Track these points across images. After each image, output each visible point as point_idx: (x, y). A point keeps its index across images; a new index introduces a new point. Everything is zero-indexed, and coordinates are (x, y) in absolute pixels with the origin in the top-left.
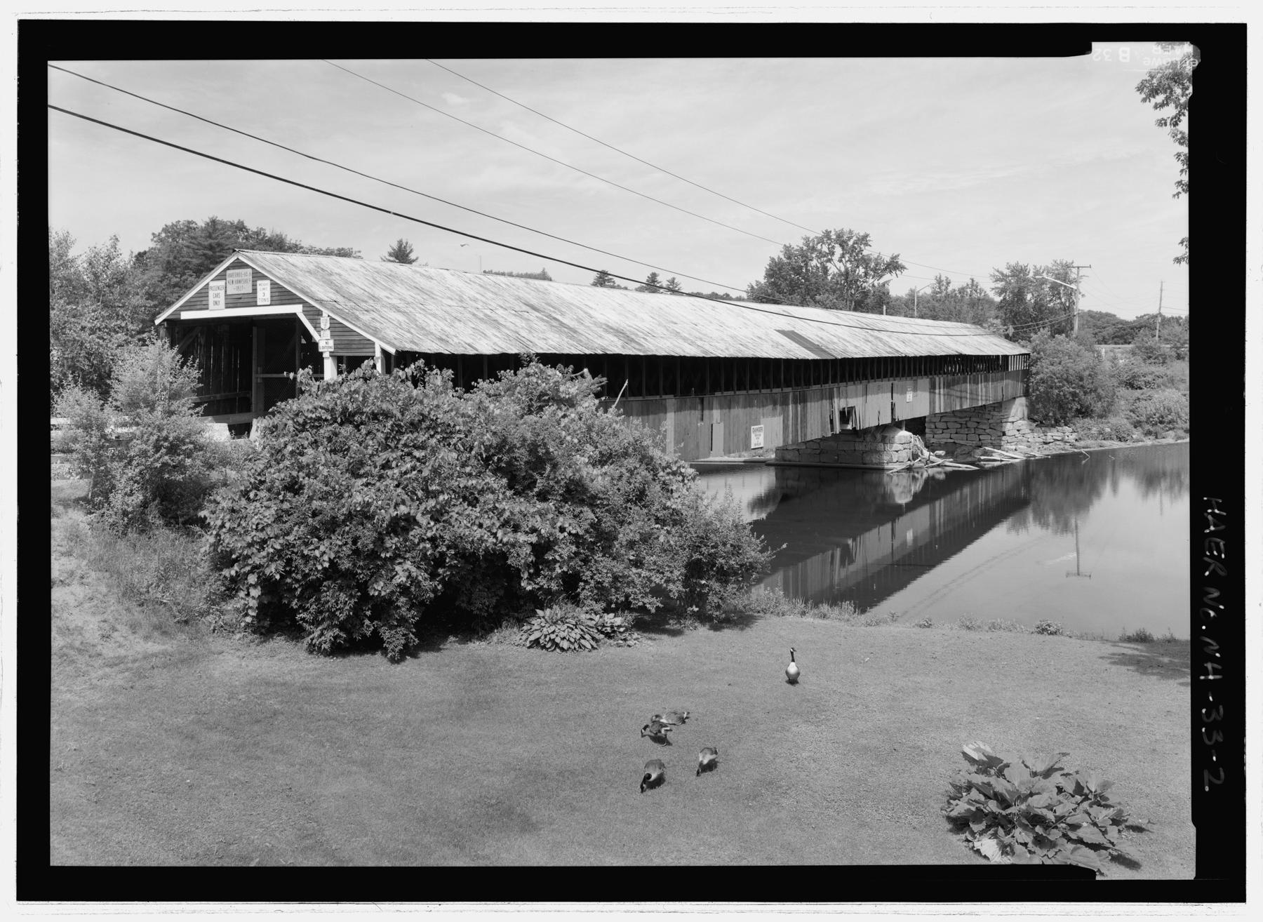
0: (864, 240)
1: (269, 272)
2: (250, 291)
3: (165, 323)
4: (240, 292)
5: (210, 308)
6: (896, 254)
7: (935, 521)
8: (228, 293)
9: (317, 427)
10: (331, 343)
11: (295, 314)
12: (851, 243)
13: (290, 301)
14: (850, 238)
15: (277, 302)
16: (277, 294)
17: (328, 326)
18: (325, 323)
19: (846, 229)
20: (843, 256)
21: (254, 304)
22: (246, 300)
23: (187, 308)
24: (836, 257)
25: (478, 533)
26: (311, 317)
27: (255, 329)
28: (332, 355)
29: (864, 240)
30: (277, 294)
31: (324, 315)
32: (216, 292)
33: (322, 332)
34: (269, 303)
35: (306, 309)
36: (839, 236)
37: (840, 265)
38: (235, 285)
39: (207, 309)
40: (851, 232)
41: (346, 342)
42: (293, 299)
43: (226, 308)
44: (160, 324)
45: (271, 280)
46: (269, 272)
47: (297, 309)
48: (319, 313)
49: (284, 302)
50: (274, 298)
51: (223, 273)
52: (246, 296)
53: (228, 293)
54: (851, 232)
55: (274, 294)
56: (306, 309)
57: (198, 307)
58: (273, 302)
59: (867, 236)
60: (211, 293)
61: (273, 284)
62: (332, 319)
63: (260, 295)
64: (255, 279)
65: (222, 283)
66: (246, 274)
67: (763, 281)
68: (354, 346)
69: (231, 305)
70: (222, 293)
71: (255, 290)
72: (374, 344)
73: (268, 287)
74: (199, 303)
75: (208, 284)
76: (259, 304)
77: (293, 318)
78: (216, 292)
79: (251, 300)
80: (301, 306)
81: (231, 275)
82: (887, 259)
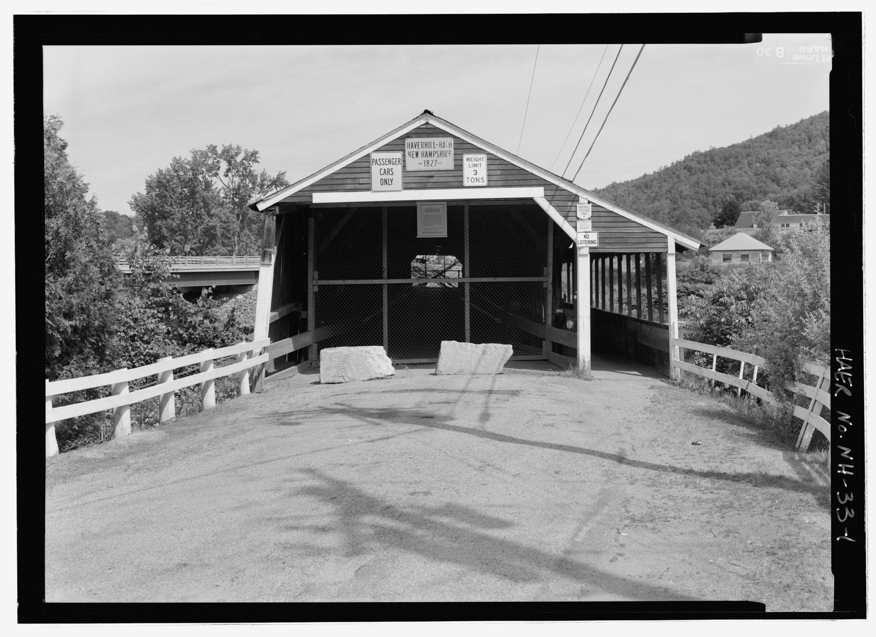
0: (253, 156)
1: (362, 148)
2: (451, 166)
3: (277, 209)
4: (430, 168)
5: (374, 188)
6: (282, 172)
7: (376, 414)
8: (409, 168)
9: (168, 319)
10: (594, 236)
11: (531, 199)
12: (239, 159)
13: (521, 182)
14: (237, 154)
15: (499, 183)
16: (498, 172)
17: (590, 214)
18: (584, 211)
19: (235, 146)
20: (228, 170)
21: (456, 184)
22: (442, 180)
23: (325, 187)
24: (221, 172)
25: (414, 436)
26: (560, 203)
27: (312, 221)
28: (595, 256)
29: (253, 156)
30: (498, 172)
31: (581, 200)
32: (386, 167)
33: (579, 223)
34: (485, 184)
35: (550, 193)
36: (226, 151)
37: (226, 181)
38: (421, 159)
39: (369, 189)
40: (238, 148)
41: (618, 235)
42: (526, 178)
43: (405, 189)
44: (267, 210)
45: (488, 154)
46: (362, 148)
47: (537, 194)
48: (575, 199)
49: (509, 183)
50: (494, 178)
51: (399, 142)
52: (443, 174)
53: (409, 168)
54: (238, 148)
55: (493, 173)
56: (550, 193)
57: (348, 187)
58: (492, 183)
59: (256, 153)
60: (375, 169)
61: (492, 159)
62: (595, 205)
63: (468, 172)
64: (459, 152)
65: (398, 155)
66: (442, 145)
67: (144, 192)
68: (631, 240)
69: (414, 186)
70: (398, 169)
71: (459, 167)
72: (666, 237)
73: (484, 163)
74: (350, 181)
75: (368, 156)
76: (466, 184)
77: (529, 207)
78: (386, 167)
79: (455, 179)
80: (542, 189)
81: (412, 145)
82: (274, 175)
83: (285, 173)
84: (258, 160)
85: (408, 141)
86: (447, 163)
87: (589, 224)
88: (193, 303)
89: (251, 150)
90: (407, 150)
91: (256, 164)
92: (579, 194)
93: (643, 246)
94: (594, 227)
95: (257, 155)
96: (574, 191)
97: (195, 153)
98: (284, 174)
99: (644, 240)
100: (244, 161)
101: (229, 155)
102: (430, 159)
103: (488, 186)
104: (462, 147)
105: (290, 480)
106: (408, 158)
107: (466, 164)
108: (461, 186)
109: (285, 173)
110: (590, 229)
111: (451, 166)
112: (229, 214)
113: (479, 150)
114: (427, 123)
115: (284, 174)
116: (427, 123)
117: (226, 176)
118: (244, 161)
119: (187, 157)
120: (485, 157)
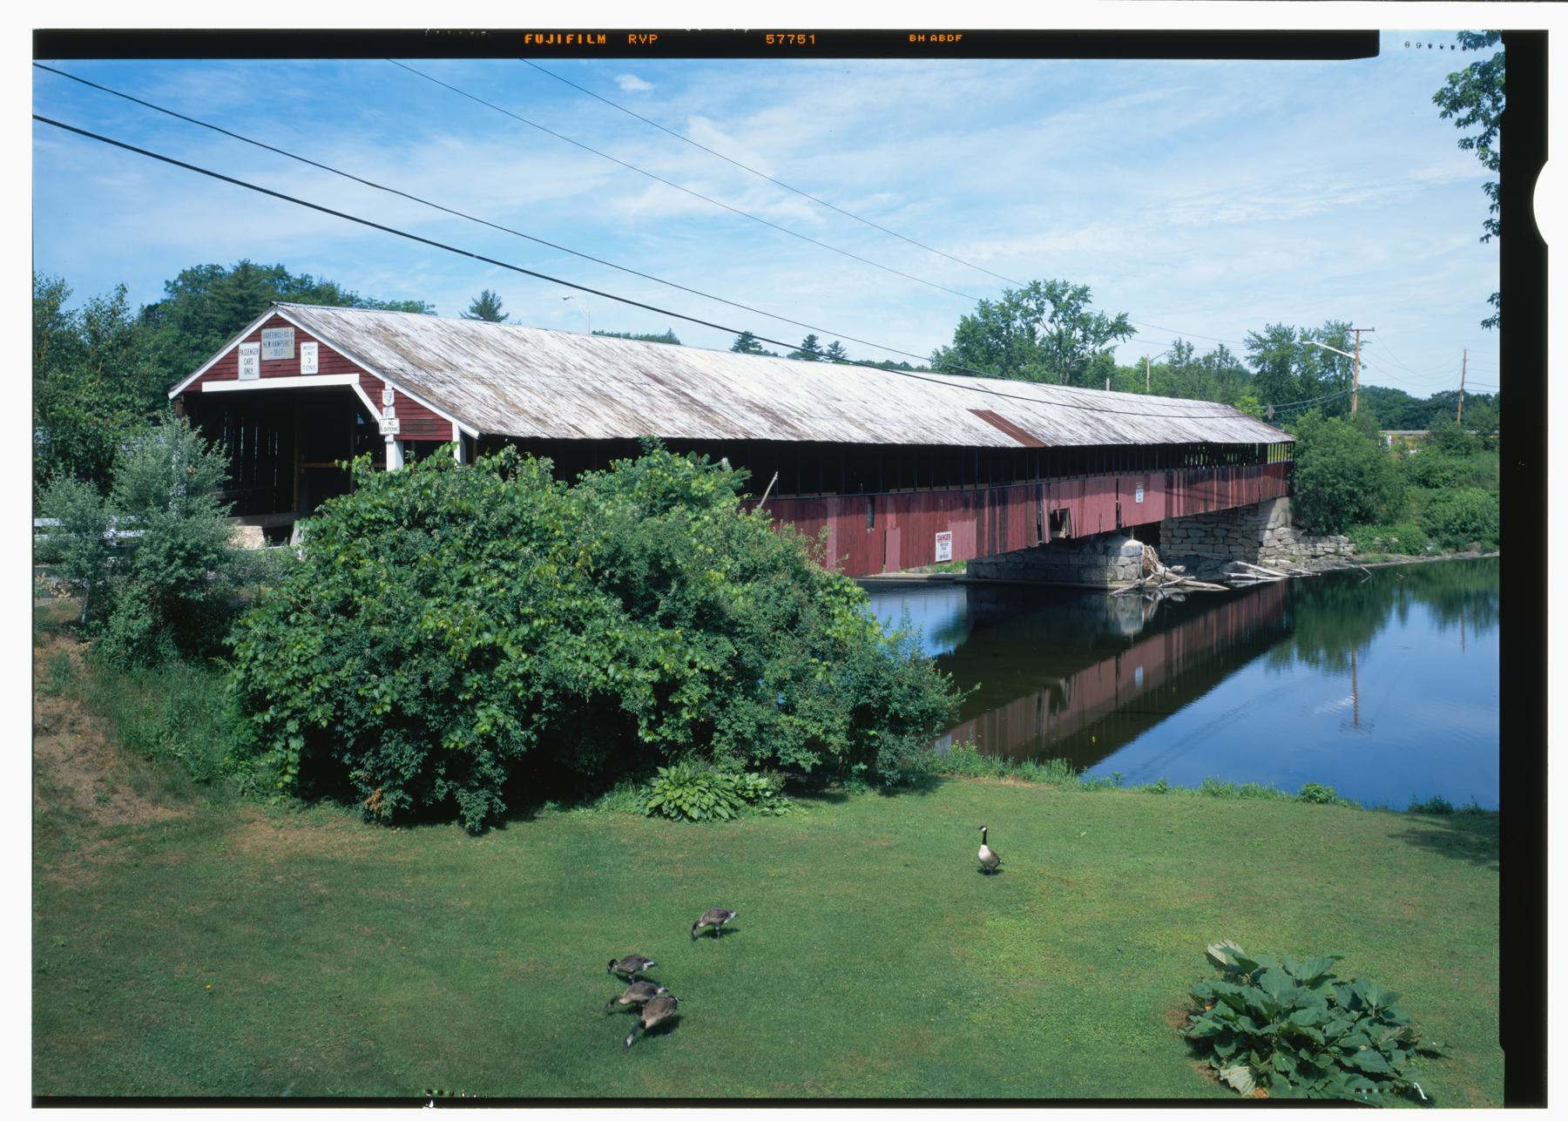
0: (1082, 294)
2: (292, 356)
10: (396, 423)
12: (1065, 298)
14: (1064, 292)
17: (392, 401)
18: (388, 398)
19: (1060, 281)
20: (1055, 314)
23: (210, 377)
29: (1082, 294)
31: (387, 387)
37: (1050, 326)
38: (272, 349)
40: (1065, 284)
47: (352, 380)
48: (381, 385)
54: (1065, 284)
56: (364, 379)
65: (256, 345)
66: (286, 334)
70: (256, 359)
73: (316, 351)
74: (225, 371)
75: (237, 347)
76: (303, 372)
77: (347, 391)
79: (292, 368)
81: (268, 336)
82: (1112, 319)
84: (1089, 298)
85: (264, 332)
86: (289, 354)
87: (392, 410)
88: (346, 492)
89: (1080, 286)
90: (263, 340)
91: (1087, 304)
92: (385, 380)
95: (1088, 293)
99: (434, 428)
100: (1072, 301)
101: (1053, 294)
103: (319, 374)
105: (1393, 811)
106: (264, 349)
107: (303, 352)
108: (297, 373)
110: (393, 416)
111: (292, 356)
112: (1044, 372)
113: (311, 339)
114: (276, 314)
116: (276, 314)
117: (1052, 321)
118: (1072, 301)
119: (997, 298)
120: (315, 345)
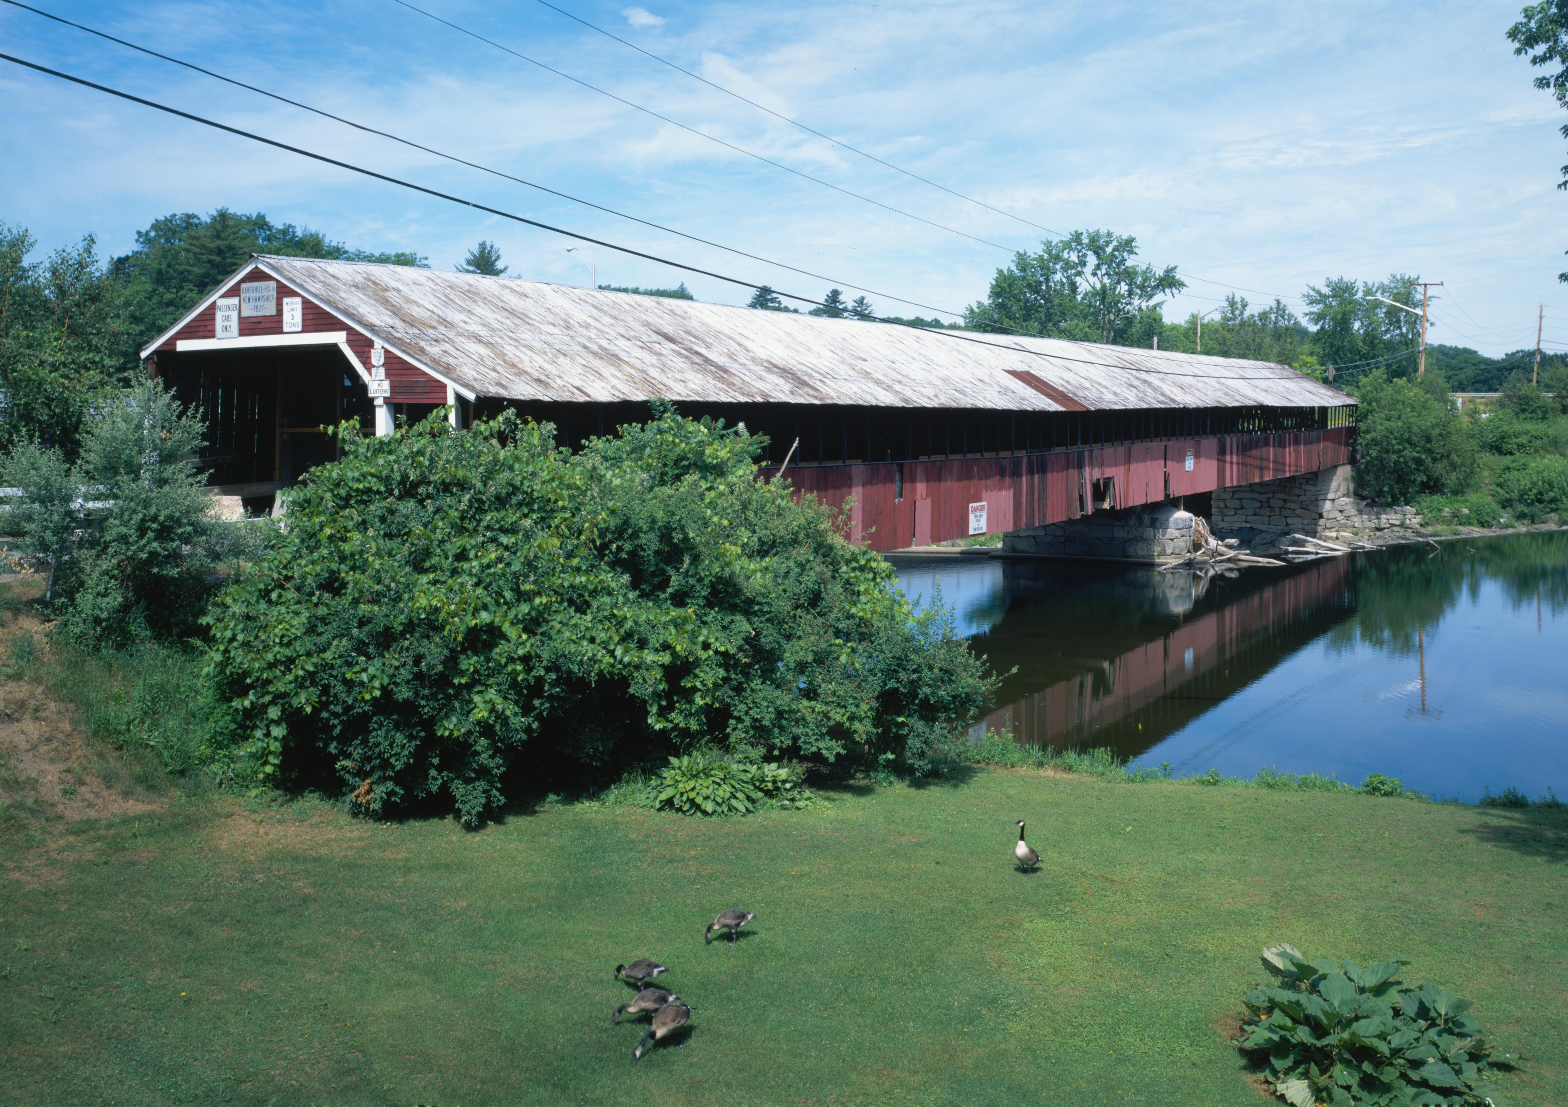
0: (1128, 245)
2: (274, 312)
10: (386, 385)
12: (1109, 250)
14: (1108, 243)
17: (382, 361)
18: (377, 357)
19: (1103, 231)
20: (1098, 267)
29: (1128, 245)
31: (376, 346)
37: (1092, 280)
38: (252, 304)
40: (1109, 234)
47: (338, 338)
48: (370, 344)
54: (1109, 234)
60: (219, 315)
70: (234, 315)
75: (214, 303)
76: (286, 329)
79: (274, 325)
81: (247, 290)
83: (1175, 268)
84: (1135, 250)
85: (244, 286)
86: (270, 310)
87: (382, 371)
90: (242, 295)
92: (374, 338)
93: (426, 396)
94: (388, 376)
96: (368, 334)
97: (1048, 244)
98: (1174, 269)
100: (1116, 253)
101: (1096, 245)
102: (259, 304)
103: (303, 331)
104: (283, 292)
106: (243, 304)
107: (286, 308)
109: (1175, 268)
111: (274, 312)
115: (1174, 269)
118: (1116, 253)
119: (1035, 250)
120: (299, 300)
